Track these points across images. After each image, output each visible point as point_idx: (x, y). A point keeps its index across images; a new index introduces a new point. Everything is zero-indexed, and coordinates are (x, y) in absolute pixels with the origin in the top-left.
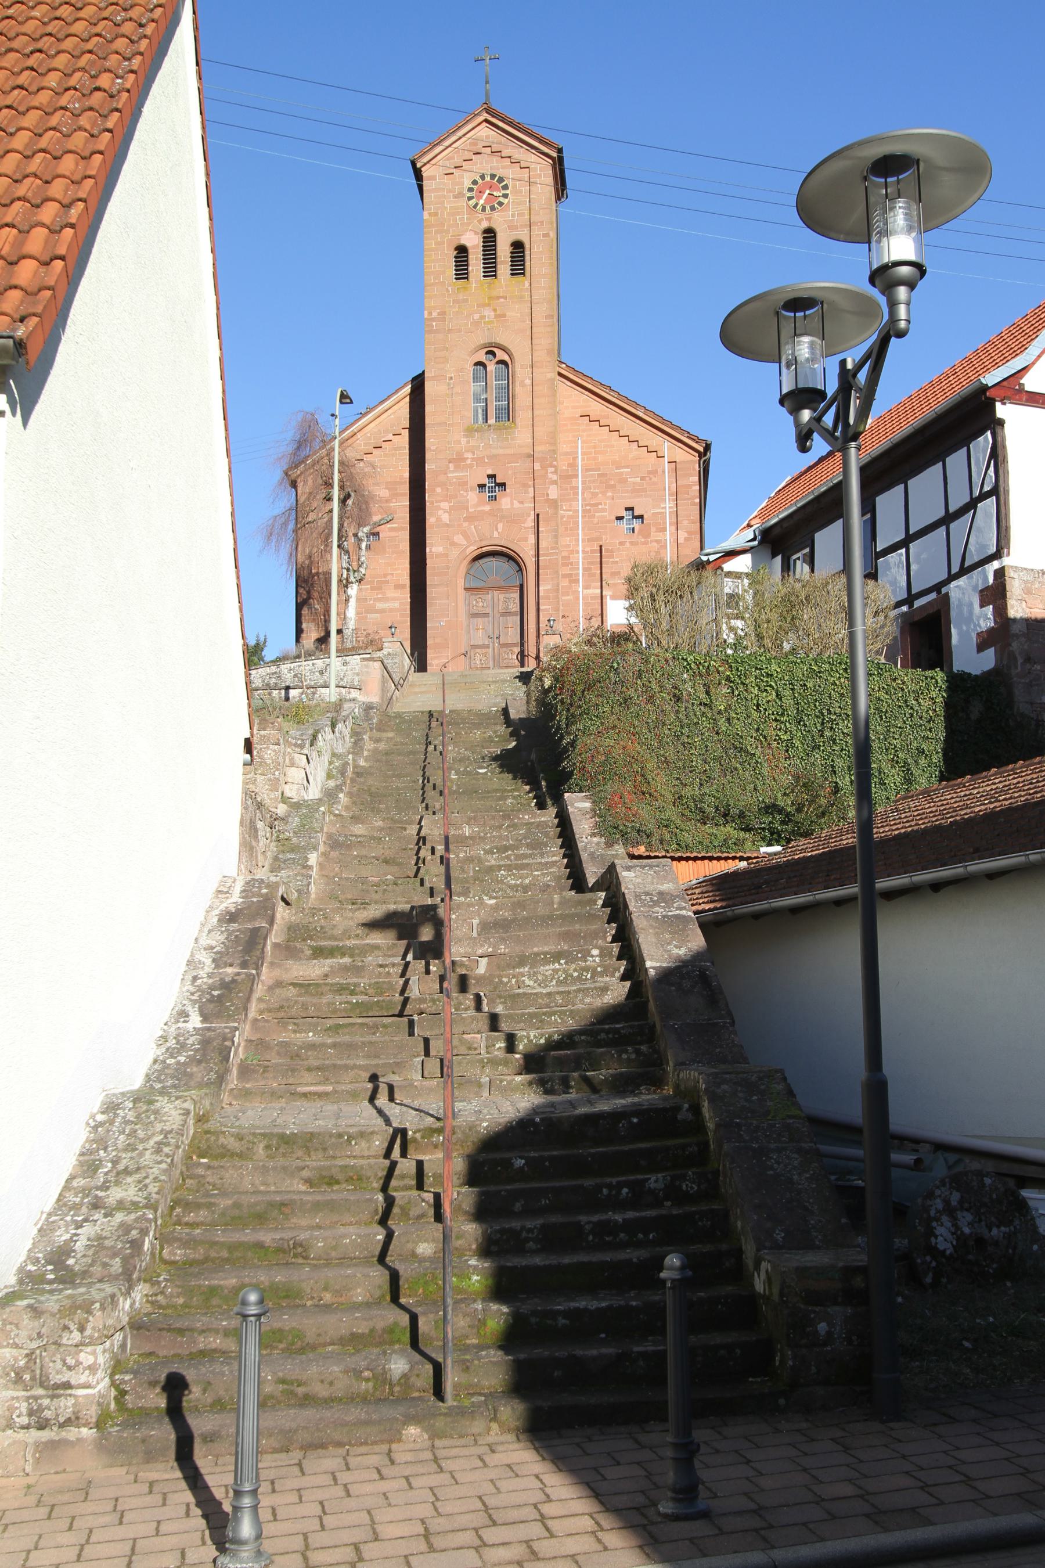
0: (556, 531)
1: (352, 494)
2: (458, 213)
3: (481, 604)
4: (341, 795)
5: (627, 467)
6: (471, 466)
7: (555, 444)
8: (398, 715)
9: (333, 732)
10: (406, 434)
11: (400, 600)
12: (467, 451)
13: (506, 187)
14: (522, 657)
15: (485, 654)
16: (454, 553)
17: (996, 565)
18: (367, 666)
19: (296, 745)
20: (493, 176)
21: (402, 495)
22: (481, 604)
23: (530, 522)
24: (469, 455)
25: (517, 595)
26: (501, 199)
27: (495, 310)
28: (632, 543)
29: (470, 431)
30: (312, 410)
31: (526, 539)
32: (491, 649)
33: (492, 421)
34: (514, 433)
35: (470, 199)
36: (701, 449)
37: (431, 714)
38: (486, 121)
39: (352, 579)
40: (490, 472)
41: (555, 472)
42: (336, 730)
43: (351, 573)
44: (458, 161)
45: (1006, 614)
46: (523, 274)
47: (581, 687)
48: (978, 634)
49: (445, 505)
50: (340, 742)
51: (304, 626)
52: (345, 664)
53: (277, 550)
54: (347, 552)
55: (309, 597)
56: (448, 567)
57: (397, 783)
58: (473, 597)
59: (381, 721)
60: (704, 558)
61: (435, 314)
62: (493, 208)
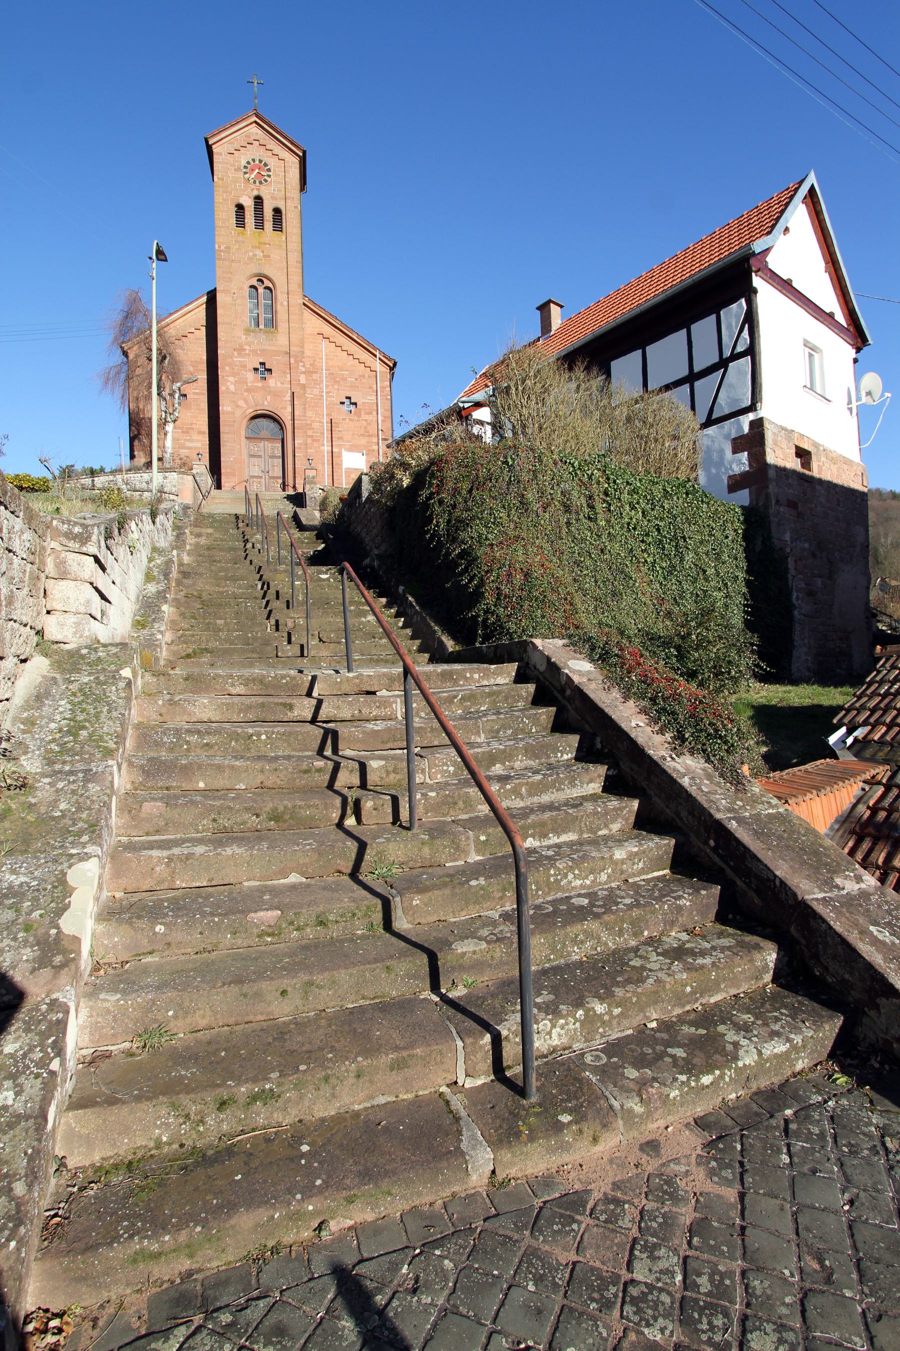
4: (165, 608)
6: (249, 355)
7: (303, 347)
8: (211, 516)
9: (154, 523)
10: (204, 329)
11: (202, 443)
14: (284, 487)
15: (260, 483)
16: (238, 413)
17: (751, 416)
18: (182, 478)
19: (70, 536)
20: (260, 161)
23: (288, 397)
24: (247, 347)
25: (280, 445)
26: (266, 178)
31: (285, 408)
33: (262, 326)
35: (245, 173)
37: (237, 517)
38: (256, 122)
39: (169, 419)
40: (261, 361)
41: (304, 366)
42: (157, 520)
45: (765, 460)
47: (466, 486)
48: (730, 477)
49: (231, 379)
50: (162, 535)
51: (136, 453)
54: (165, 399)
55: (139, 434)
57: (232, 588)
59: (197, 519)
60: (461, 405)
61: (222, 248)
62: (261, 183)
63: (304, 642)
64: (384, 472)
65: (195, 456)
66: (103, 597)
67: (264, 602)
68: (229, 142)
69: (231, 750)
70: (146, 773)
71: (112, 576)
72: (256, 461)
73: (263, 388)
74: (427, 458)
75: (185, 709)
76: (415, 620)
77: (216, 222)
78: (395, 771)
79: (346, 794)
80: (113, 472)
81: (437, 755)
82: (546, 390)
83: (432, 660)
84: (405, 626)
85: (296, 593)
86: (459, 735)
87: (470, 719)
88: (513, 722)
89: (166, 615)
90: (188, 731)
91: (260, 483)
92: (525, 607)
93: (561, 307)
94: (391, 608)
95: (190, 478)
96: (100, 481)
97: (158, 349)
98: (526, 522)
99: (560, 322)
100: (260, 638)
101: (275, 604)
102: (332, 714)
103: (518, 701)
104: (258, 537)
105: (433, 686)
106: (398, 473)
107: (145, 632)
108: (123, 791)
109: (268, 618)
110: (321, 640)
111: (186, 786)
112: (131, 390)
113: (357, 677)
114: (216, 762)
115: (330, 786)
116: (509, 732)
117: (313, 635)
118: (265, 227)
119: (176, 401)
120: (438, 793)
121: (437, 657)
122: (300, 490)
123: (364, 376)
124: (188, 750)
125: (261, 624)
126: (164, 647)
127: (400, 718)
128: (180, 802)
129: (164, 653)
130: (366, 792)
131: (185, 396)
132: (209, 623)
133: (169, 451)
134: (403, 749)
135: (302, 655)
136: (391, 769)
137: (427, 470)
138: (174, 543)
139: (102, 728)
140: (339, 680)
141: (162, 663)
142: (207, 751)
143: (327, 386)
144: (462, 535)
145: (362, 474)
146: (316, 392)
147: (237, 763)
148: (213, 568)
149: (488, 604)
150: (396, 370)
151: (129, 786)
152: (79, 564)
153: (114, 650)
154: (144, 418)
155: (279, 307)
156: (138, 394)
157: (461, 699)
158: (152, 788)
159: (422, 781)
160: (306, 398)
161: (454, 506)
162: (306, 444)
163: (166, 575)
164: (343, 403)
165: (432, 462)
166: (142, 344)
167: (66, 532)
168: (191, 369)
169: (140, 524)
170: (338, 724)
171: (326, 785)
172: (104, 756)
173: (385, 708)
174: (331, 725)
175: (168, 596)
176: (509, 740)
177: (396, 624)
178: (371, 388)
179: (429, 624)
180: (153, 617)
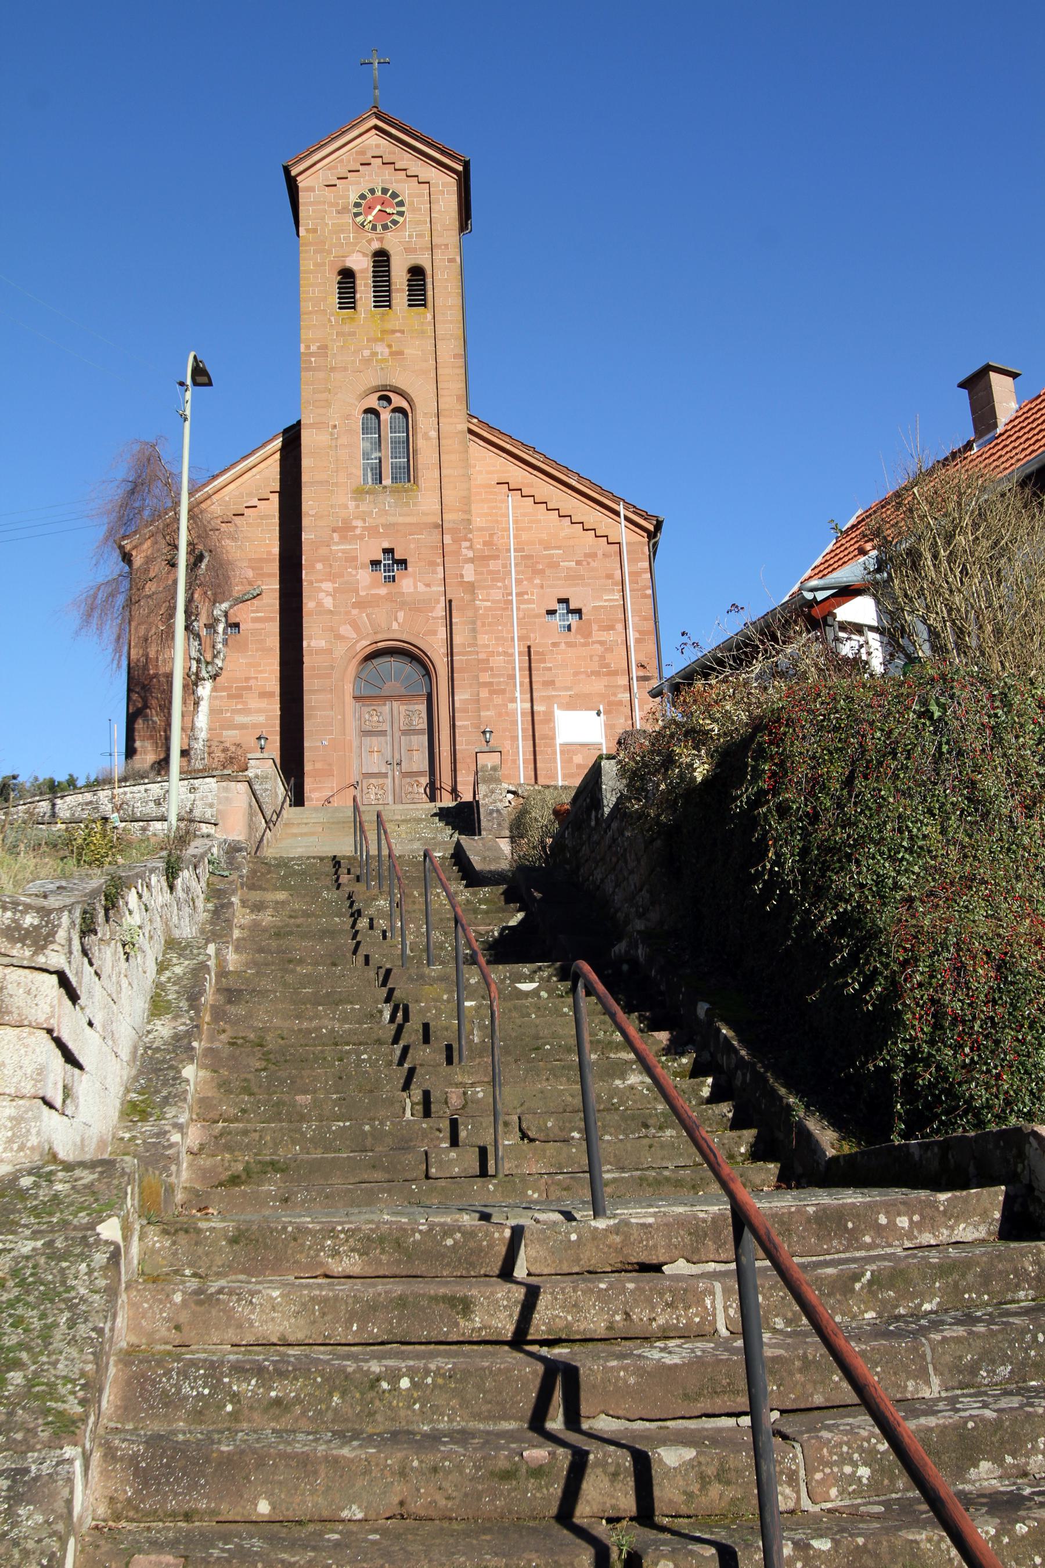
0: (474, 623)
1: (206, 554)
2: (343, 231)
3: (375, 718)
4: (189, 1071)
5: (559, 548)
7: (468, 512)
8: (283, 863)
9: (171, 887)
10: (275, 498)
12: (357, 518)
13: (401, 204)
15: (382, 787)
16: (340, 650)
18: (226, 789)
20: (385, 191)
21: (270, 575)
22: (375, 718)
23: (440, 611)
24: (359, 523)
25: (423, 708)
26: (395, 217)
27: (390, 346)
28: (566, 643)
29: (359, 493)
30: (152, 439)
31: (434, 633)
32: (389, 780)
33: (387, 481)
34: (417, 497)
35: (356, 215)
36: (651, 528)
37: (336, 862)
39: (204, 674)
40: (386, 545)
41: (471, 548)
42: (179, 882)
43: (203, 666)
44: (342, 171)
46: (424, 305)
47: (837, 771)
49: (327, 586)
50: (187, 910)
52: (193, 790)
53: (100, 629)
55: (146, 706)
56: (332, 667)
57: (328, 1023)
58: (365, 709)
59: (253, 872)
60: (809, 596)
61: (313, 348)
62: (385, 227)
63: (487, 1140)
64: (652, 752)
65: (253, 742)
66: (70, 1058)
67: (398, 1049)
68: (329, 168)
69: (330, 1415)
70: (143, 1476)
71: (87, 1011)
72: (375, 742)
73: (389, 598)
74: (744, 717)
75: (229, 1313)
76: (738, 1082)
77: (302, 304)
78: (722, 1476)
79: (603, 1537)
80: (94, 785)
81: (825, 1434)
82: (1000, 550)
83: (787, 1180)
84: (715, 1098)
85: (467, 1027)
86: (874, 1376)
87: (898, 1334)
88: (1011, 1342)
89: (191, 1088)
90: (239, 1370)
91: (382, 787)
92: (1006, 1045)
93: (1014, 375)
94: (682, 1054)
95: (243, 787)
96: (66, 805)
97: (190, 544)
98: (988, 842)
99: (1014, 406)
100: (390, 1132)
101: (423, 1055)
102: (560, 1324)
103: (1018, 1287)
104: (382, 903)
105: (797, 1248)
106: (684, 754)
107: (147, 1127)
108: (89, 1522)
109: (406, 1087)
110: (524, 1136)
111: (228, 1510)
112: (133, 624)
113: (616, 1230)
114: (299, 1448)
115: (565, 1515)
116: (1005, 1371)
117: (506, 1124)
118: (394, 302)
119: (220, 638)
120: (836, 1543)
121: (799, 1170)
122: (467, 797)
123: (593, 555)
124: (235, 1416)
125: (391, 1102)
126: (185, 1160)
127: (724, 1332)
128: (216, 1553)
129: (185, 1175)
130: (652, 1534)
131: (237, 625)
132: (279, 1103)
133: (203, 735)
134: (738, 1415)
135: (484, 1173)
136: (710, 1471)
137: (746, 742)
138: (208, 927)
139: (54, 1364)
140: (574, 1237)
141: (179, 1197)
142: (276, 1419)
143: (519, 582)
144: (839, 881)
145: (600, 757)
146: (497, 594)
147: (345, 1451)
148: (289, 978)
149: (913, 1039)
150: (661, 537)
151: (102, 1510)
152: (29, 993)
153: (87, 1177)
154: (156, 675)
155: (421, 443)
156: (148, 630)
157: (870, 1282)
158: (153, 1515)
159: (791, 1505)
160: (477, 609)
161: (814, 818)
162: (478, 701)
163: (193, 998)
164: (551, 612)
165: (758, 725)
166: (160, 537)
167: (8, 927)
168: (250, 574)
169: (146, 893)
170: (577, 1347)
171: (554, 1510)
172: (56, 1435)
173: (687, 1308)
174: (560, 1352)
175: (195, 1044)
176: (1006, 1393)
177: (696, 1091)
178: (609, 576)
179: (774, 1091)
180: (164, 1093)
